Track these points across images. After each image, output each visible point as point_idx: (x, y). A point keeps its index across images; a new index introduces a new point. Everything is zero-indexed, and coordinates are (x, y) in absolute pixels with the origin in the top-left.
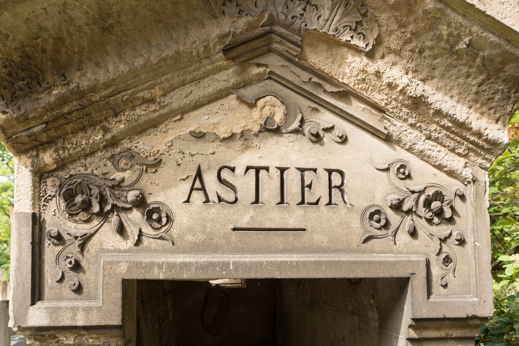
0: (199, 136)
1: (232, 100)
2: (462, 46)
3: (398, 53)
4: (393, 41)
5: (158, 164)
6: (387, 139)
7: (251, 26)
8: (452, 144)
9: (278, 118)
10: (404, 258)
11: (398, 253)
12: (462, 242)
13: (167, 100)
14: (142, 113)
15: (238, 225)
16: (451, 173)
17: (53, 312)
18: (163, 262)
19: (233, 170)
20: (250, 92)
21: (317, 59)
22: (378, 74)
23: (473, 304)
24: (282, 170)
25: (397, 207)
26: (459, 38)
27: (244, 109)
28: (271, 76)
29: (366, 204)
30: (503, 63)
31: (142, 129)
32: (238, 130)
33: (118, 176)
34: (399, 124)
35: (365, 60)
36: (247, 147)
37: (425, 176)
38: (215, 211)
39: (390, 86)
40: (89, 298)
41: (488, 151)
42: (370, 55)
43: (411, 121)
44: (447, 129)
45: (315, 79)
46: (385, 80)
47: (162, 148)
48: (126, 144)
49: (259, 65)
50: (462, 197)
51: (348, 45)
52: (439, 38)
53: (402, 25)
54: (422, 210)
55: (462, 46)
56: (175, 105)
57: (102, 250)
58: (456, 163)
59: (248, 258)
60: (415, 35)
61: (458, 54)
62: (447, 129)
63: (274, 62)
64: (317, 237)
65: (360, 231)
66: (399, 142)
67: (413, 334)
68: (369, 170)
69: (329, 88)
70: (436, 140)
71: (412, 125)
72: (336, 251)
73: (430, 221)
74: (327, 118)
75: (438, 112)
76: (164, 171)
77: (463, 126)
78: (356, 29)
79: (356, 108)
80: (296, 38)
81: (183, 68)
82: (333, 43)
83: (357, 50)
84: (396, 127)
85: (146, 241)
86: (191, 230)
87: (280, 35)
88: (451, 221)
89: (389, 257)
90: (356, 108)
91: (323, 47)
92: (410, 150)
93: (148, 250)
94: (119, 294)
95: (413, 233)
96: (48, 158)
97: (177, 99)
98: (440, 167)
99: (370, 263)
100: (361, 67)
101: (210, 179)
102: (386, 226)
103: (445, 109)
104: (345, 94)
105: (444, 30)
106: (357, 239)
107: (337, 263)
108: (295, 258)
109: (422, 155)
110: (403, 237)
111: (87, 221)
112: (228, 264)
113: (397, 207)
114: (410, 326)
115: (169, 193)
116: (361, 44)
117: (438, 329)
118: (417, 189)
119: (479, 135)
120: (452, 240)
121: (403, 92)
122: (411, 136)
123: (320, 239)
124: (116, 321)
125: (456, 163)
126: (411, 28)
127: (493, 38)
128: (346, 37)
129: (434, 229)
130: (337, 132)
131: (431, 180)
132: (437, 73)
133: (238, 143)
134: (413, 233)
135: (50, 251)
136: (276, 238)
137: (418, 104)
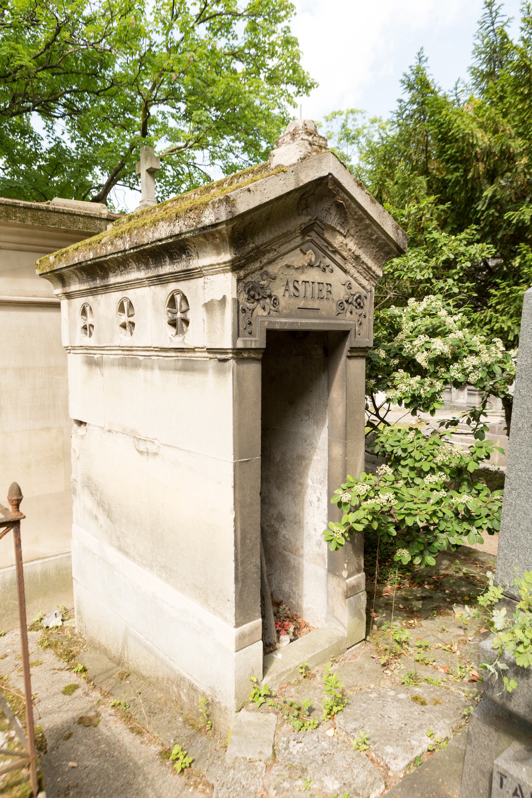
0: (288, 266)
1: (298, 251)
2: (374, 237)
3: (353, 236)
4: (352, 232)
5: (274, 279)
6: (345, 271)
7: (310, 220)
8: (365, 275)
9: (313, 259)
10: (348, 322)
11: (347, 320)
12: (365, 316)
13: (280, 250)
14: (271, 256)
15: (300, 306)
16: (363, 287)
17: (245, 342)
18: (283, 322)
19: (298, 282)
20: (304, 247)
21: (327, 236)
22: (346, 245)
23: (368, 342)
24: (313, 283)
25: (347, 301)
26: (373, 235)
27: (302, 255)
28: (312, 241)
29: (338, 299)
30: (385, 246)
31: (270, 262)
32: (300, 265)
33: (262, 283)
34: (350, 265)
35: (343, 238)
36: (303, 272)
37: (356, 288)
38: (292, 300)
39: (350, 250)
40: (255, 336)
41: (376, 279)
42: (345, 236)
43: (354, 264)
44: (365, 269)
45: (325, 244)
46: (348, 247)
47: (276, 271)
48: (265, 269)
49: (308, 236)
50: (366, 298)
51: (339, 231)
52: (367, 233)
53: (356, 226)
54: (354, 303)
55: (374, 237)
56: (282, 252)
57: (258, 316)
58: (365, 283)
59: (304, 321)
60: (360, 230)
61: (372, 240)
62: (365, 269)
63: (313, 234)
64: (323, 312)
65: (335, 310)
66: (349, 273)
67: (349, 354)
68: (339, 284)
69: (331, 249)
70: (360, 273)
71: (354, 266)
72: (328, 319)
73: (356, 307)
74: (328, 261)
75: (363, 262)
76: (277, 281)
77: (370, 268)
78: (342, 225)
79: (337, 258)
80: (323, 227)
81: (287, 236)
82: (334, 230)
83: (341, 234)
84: (348, 267)
85: (272, 312)
86: (285, 308)
87: (318, 225)
88: (362, 307)
89: (343, 322)
90: (337, 258)
91: (330, 231)
92: (352, 276)
93: (272, 316)
94: (265, 335)
95: (351, 313)
96: (242, 273)
97: (283, 249)
98: (360, 284)
99: (339, 324)
100: (341, 241)
101: (291, 285)
102: (343, 309)
103: (365, 262)
104: (335, 252)
105: (370, 231)
106: (334, 314)
107: (330, 324)
108: (317, 321)
109: (355, 279)
110: (348, 314)
111: (253, 303)
112: (298, 323)
113: (347, 301)
114: (349, 351)
115: (278, 291)
116: (343, 232)
117: (356, 352)
118: (353, 293)
119: (374, 272)
120: (362, 316)
121: (353, 253)
122: (353, 271)
123: (323, 313)
124: (264, 346)
125: (365, 283)
126: (359, 227)
127: (384, 237)
128: (338, 229)
129: (357, 311)
130: (330, 267)
131: (357, 290)
132: (364, 245)
133: (300, 271)
134: (351, 313)
135: (242, 315)
136: (311, 313)
137: (357, 258)
